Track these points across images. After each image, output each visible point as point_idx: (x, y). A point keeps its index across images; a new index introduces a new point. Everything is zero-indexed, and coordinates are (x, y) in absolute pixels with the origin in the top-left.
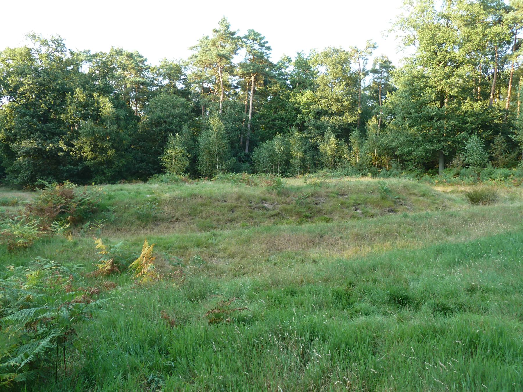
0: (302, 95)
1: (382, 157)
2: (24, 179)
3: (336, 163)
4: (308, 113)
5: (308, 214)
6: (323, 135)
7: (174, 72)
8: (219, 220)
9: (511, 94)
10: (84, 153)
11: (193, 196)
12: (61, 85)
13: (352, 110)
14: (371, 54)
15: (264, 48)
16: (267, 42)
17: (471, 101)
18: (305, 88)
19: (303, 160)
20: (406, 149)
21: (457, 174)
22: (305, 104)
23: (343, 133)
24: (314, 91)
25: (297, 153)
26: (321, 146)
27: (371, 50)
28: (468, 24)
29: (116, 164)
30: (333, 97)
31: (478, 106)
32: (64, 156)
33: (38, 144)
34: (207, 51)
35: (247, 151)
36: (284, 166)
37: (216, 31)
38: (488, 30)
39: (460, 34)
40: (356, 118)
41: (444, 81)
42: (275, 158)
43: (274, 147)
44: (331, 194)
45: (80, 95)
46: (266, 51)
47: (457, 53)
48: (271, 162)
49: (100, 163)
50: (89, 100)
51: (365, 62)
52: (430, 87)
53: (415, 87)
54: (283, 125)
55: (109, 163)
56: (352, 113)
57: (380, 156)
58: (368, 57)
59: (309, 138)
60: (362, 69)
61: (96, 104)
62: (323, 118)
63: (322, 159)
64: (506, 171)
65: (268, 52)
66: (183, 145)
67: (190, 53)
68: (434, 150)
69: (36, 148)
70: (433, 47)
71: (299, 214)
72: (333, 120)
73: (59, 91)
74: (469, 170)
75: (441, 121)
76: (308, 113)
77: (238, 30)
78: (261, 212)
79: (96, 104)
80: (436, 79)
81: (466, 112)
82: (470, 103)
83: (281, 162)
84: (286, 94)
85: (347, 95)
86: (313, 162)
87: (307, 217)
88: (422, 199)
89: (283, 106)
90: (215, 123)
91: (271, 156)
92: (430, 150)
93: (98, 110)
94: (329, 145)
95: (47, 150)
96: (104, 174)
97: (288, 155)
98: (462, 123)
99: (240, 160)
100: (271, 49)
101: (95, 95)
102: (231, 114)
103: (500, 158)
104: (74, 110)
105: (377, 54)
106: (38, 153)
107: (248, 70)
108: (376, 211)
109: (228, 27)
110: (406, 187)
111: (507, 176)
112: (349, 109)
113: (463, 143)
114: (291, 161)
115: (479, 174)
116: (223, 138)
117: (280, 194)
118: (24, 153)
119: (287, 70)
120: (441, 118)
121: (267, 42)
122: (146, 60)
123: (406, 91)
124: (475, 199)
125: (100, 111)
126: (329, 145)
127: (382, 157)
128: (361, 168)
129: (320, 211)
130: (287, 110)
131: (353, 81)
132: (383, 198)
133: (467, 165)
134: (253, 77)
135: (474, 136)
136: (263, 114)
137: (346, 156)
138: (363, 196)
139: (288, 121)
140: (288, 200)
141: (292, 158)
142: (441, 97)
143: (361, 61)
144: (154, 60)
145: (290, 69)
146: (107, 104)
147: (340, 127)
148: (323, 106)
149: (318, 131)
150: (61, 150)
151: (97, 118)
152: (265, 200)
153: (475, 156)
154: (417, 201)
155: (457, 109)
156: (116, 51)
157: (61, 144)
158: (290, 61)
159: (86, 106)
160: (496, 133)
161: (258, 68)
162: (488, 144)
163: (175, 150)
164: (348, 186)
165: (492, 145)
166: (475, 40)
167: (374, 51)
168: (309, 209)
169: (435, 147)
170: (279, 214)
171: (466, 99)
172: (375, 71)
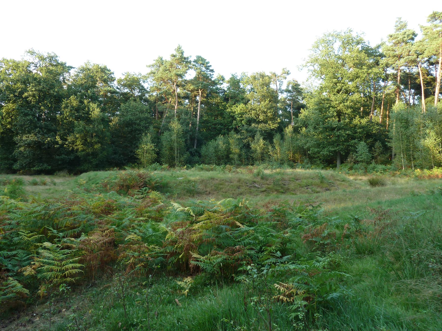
0: (237, 107)
1: (296, 155)
2: (22, 165)
3: (264, 157)
4: (241, 121)
5: (282, 190)
6: (253, 137)
7: (133, 83)
8: (233, 193)
9: (383, 112)
10: (76, 146)
11: (213, 179)
12: (57, 92)
13: (273, 119)
14: (286, 78)
15: (208, 70)
16: (211, 66)
17: (359, 118)
18: (237, 101)
19: (240, 156)
20: (316, 150)
21: (351, 168)
22: (239, 114)
23: (268, 136)
24: (246, 104)
25: (235, 150)
26: (252, 145)
27: (285, 75)
28: (356, 65)
29: (100, 155)
30: (260, 109)
31: (364, 121)
32: (58, 148)
33: (38, 138)
34: (166, 70)
35: (195, 148)
36: (225, 159)
37: (174, 56)
38: (370, 71)
39: (353, 71)
40: (276, 125)
41: (342, 104)
42: (219, 154)
43: (218, 145)
44: (291, 179)
45: (74, 101)
46: (210, 73)
47: (351, 85)
48: (216, 156)
49: (88, 154)
50: (81, 105)
51: (281, 84)
52: (332, 107)
53: (323, 107)
54: (222, 128)
55: (94, 154)
56: (273, 121)
57: (294, 154)
58: (284, 80)
59: (242, 139)
60: (278, 88)
61: (87, 109)
62: (253, 125)
63: (254, 156)
64: (383, 166)
65: (212, 74)
66: (153, 142)
67: (149, 70)
68: (335, 151)
69: (36, 141)
70: (335, 80)
71: (277, 191)
72: (261, 126)
73: (55, 97)
74: (359, 165)
75: (340, 131)
76: (241, 121)
77: (190, 56)
78: (255, 189)
79: (87, 109)
80: (337, 102)
81: (356, 125)
82: (359, 119)
83: (223, 156)
84: (223, 105)
85: (270, 108)
86: (248, 158)
87: (282, 193)
88: (343, 183)
89: (222, 114)
90: (175, 125)
91: (216, 152)
92: (332, 151)
93: (88, 113)
94: (258, 145)
95: (46, 142)
96: (91, 163)
97: (228, 151)
98: (353, 133)
99: (192, 154)
100: (214, 72)
101: (86, 101)
102: (185, 119)
103: (379, 158)
104: (69, 112)
105: (290, 78)
106: (38, 145)
107: (197, 87)
108: (318, 189)
109: (182, 53)
110: (332, 176)
111: (385, 170)
112: (271, 118)
113: (355, 147)
114: (231, 156)
115: (366, 168)
116: (181, 138)
117: (262, 178)
118: (26, 144)
119: (222, 86)
120: (339, 129)
121: (211, 66)
122: (113, 73)
123: (316, 109)
124: (373, 183)
125: (90, 114)
126: (258, 145)
127: (296, 155)
128: (282, 162)
129: (288, 189)
130: (225, 117)
131: (273, 97)
132: (321, 182)
133: (356, 162)
134: (200, 92)
135: (362, 143)
136: (206, 120)
137: (271, 153)
138: (310, 181)
139: (225, 126)
140: (268, 182)
141: (231, 154)
142: (339, 114)
143: (278, 83)
144: (119, 74)
145: (225, 86)
146: (96, 109)
147: (265, 131)
148: (253, 115)
149: (249, 134)
150: (57, 143)
151: (88, 120)
152: (255, 182)
153: (363, 156)
154: (340, 184)
155: (350, 123)
156: (101, 68)
157: (58, 138)
158: (223, 80)
159: (77, 110)
160: (376, 140)
161: (204, 85)
162: (371, 147)
163: (146, 146)
164: (299, 175)
165: (373, 148)
166: (362, 77)
167: (287, 76)
168: (282, 188)
169: (336, 149)
170: (266, 190)
171: (355, 116)
172: (289, 91)
